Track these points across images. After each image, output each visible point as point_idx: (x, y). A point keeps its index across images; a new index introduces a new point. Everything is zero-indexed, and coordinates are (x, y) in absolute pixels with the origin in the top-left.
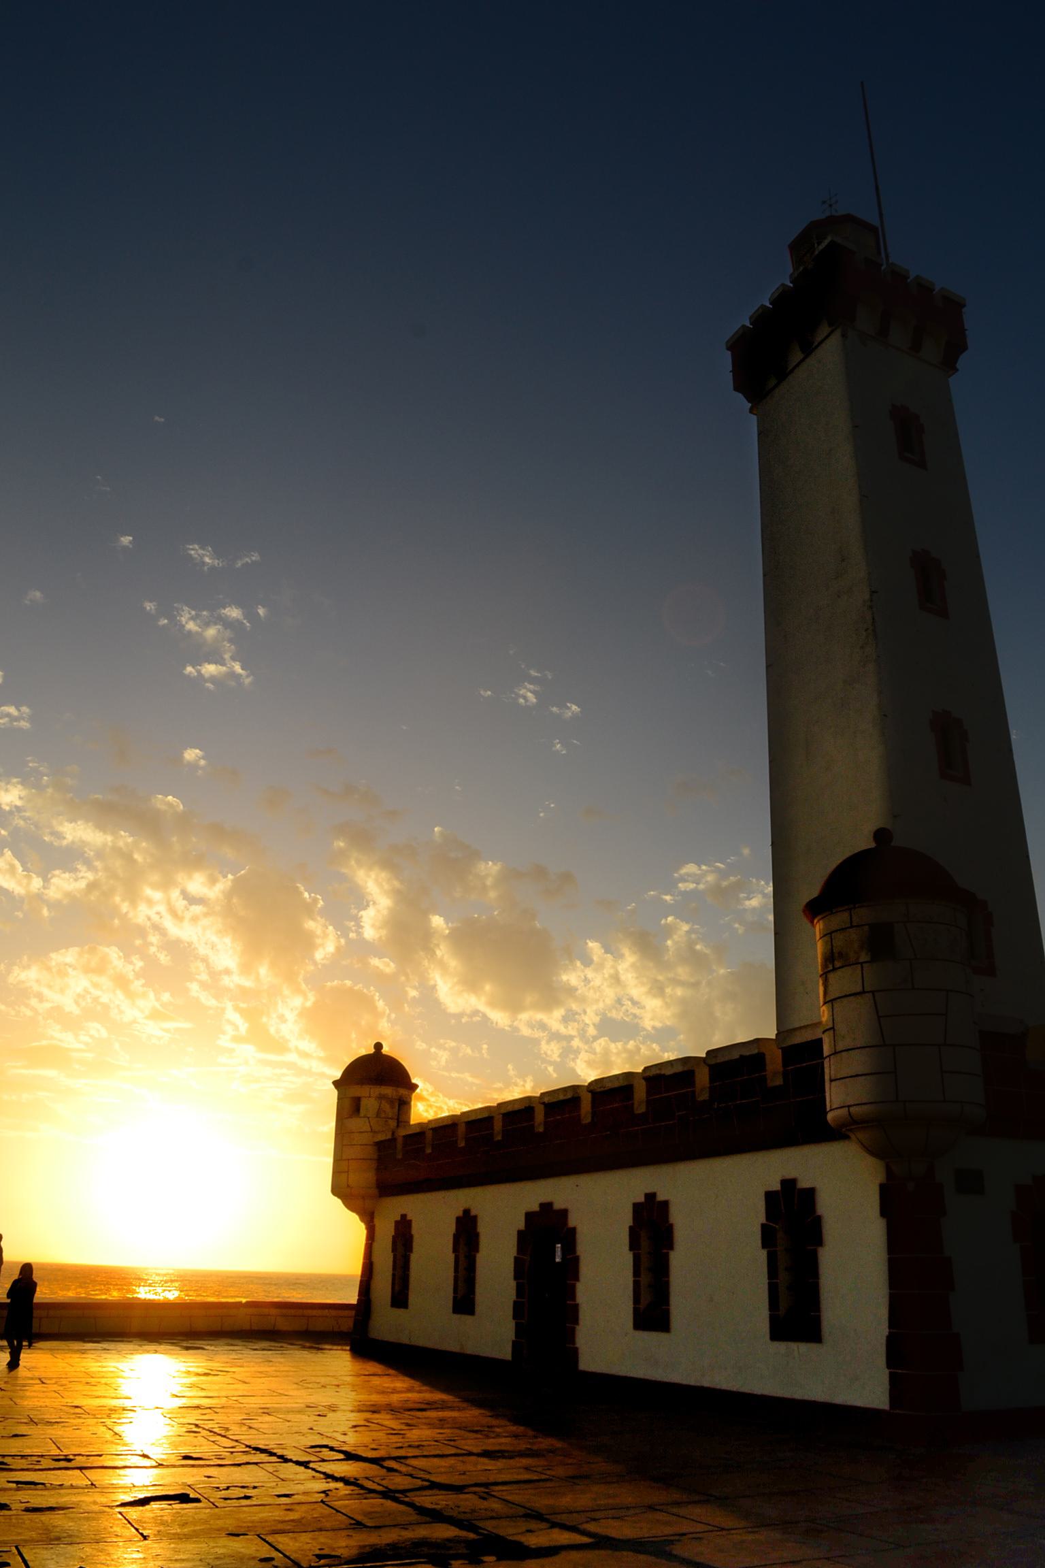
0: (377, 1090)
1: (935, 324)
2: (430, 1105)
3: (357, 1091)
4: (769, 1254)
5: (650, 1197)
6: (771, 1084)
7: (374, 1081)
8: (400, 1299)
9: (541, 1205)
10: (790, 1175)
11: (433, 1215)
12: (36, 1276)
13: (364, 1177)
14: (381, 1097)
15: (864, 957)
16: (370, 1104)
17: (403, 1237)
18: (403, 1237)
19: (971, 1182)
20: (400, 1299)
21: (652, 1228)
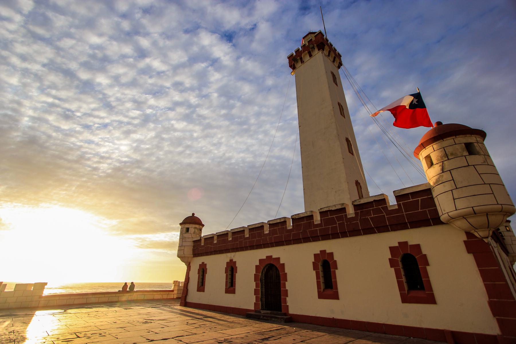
0: (194, 226)
1: (336, 59)
2: (206, 232)
3: (187, 226)
4: (316, 272)
5: (203, 263)
6: (315, 223)
7: (192, 222)
8: (201, 287)
9: (321, 251)
10: (323, 249)
11: (217, 264)
12: (134, 285)
13: (189, 251)
14: (195, 228)
16: (192, 230)
17: (203, 270)
18: (203, 270)
20: (201, 287)
21: (231, 269)
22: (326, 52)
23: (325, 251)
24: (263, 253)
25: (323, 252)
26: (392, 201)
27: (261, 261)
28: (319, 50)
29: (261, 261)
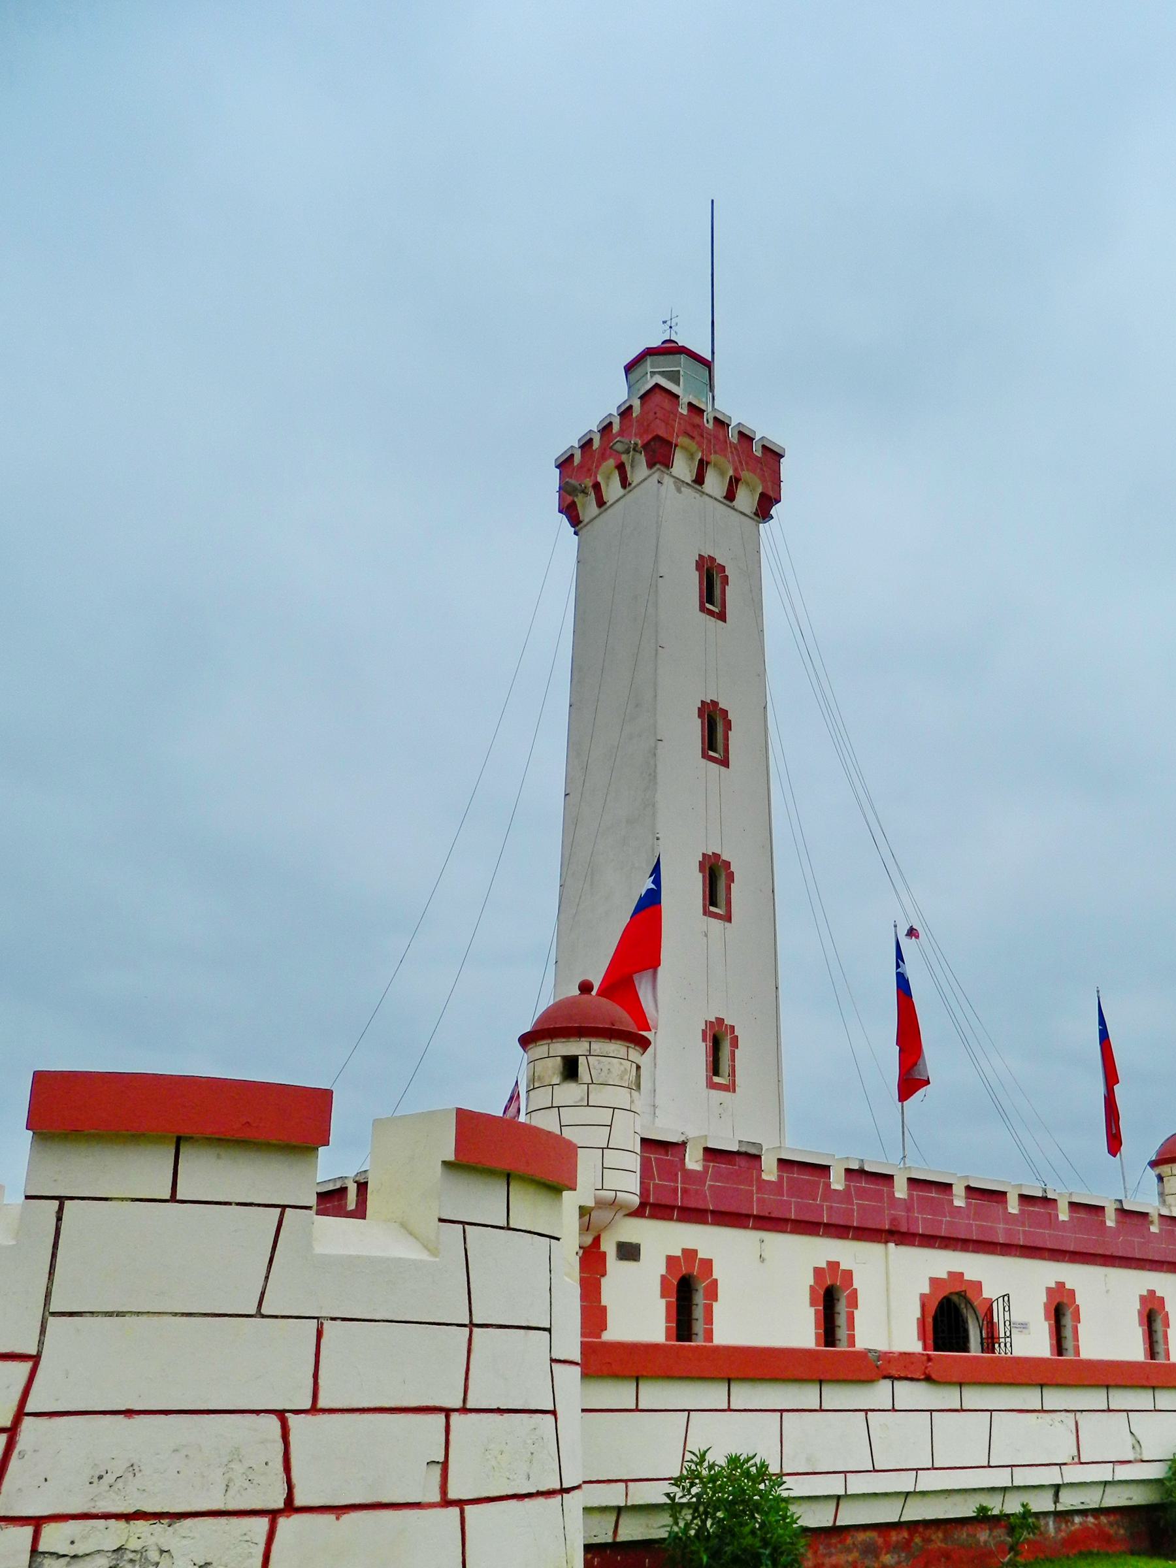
1: (754, 473)
15: (556, 1079)
19: (629, 1252)
22: (682, 467)
24: (942, 1263)
25: (690, 1254)
26: (770, 1171)
27: (934, 1281)
28: (650, 465)
29: (934, 1281)
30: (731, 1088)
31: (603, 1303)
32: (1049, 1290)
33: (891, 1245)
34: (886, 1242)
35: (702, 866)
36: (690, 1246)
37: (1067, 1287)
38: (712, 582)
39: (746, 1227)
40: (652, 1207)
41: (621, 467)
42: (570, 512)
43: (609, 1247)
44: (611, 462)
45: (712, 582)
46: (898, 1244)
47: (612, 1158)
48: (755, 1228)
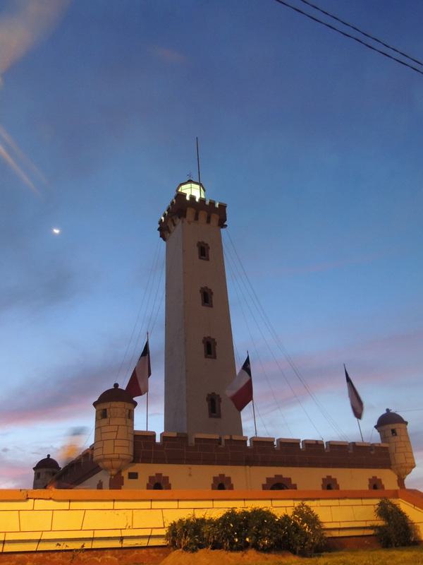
0: (45, 470)
3: (38, 471)
9: (157, 474)
19: (133, 476)
23: (161, 474)
27: (268, 479)
29: (268, 479)
30: (219, 416)
31: (274, 477)
32: (370, 480)
33: (248, 467)
34: (245, 465)
35: (203, 342)
36: (374, 475)
37: (163, 475)
38: (203, 251)
39: (183, 464)
40: (137, 458)
41: (173, 220)
42: (162, 236)
43: (125, 474)
44: (170, 219)
45: (203, 251)
46: (250, 466)
47: (117, 443)
48: (187, 464)
